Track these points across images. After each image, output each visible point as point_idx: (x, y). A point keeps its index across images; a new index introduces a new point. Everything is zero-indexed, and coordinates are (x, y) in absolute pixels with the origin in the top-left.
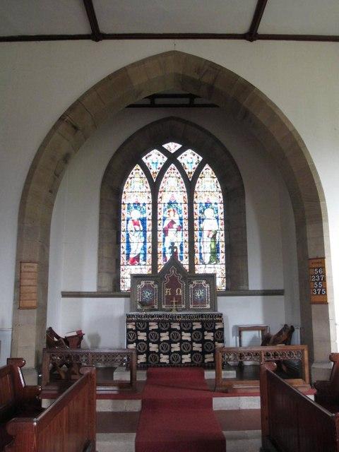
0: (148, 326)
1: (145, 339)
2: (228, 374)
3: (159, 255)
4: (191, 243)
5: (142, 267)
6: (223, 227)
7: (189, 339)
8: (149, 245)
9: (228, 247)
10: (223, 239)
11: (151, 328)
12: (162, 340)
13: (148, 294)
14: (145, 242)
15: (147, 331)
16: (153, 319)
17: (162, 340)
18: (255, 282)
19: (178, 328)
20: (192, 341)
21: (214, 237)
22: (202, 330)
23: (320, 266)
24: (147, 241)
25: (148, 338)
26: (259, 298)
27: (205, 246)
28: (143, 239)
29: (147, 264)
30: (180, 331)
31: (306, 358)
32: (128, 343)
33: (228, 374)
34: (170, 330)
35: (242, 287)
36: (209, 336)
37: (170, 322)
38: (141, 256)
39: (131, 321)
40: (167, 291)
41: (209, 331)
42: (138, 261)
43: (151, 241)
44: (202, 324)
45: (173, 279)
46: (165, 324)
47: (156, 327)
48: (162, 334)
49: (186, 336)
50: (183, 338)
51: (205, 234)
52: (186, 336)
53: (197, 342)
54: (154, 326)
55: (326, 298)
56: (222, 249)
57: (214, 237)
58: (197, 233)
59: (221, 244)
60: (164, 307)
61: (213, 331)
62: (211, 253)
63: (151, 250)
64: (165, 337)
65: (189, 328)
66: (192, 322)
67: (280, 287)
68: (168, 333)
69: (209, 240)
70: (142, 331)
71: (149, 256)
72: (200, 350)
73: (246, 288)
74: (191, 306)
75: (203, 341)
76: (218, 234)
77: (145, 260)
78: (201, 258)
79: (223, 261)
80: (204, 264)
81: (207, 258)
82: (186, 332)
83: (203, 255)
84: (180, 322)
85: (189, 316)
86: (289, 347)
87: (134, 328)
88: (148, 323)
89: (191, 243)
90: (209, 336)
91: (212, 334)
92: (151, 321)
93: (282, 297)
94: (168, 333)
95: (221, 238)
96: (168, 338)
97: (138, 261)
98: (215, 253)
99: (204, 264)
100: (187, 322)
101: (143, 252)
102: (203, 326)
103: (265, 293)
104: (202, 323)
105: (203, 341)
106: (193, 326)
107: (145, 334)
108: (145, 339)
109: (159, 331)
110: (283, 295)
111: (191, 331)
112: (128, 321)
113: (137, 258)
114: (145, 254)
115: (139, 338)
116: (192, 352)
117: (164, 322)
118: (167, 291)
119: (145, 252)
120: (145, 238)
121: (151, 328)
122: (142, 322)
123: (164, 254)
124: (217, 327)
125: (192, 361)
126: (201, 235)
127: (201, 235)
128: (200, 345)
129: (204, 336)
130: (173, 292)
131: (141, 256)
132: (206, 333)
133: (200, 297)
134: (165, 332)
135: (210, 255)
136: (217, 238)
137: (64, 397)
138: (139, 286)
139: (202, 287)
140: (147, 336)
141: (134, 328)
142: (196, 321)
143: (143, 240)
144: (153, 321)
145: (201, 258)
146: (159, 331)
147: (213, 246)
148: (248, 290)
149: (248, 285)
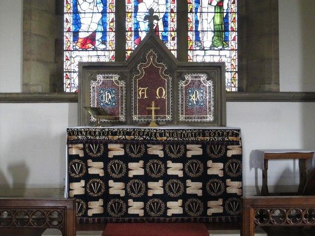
0: (107, 150)
9: (241, 20)
11: (111, 155)
12: (131, 174)
14: (104, 13)
15: (104, 158)
16: (116, 138)
17: (131, 174)
19: (161, 154)
26: (296, 106)
30: (164, 160)
34: (147, 158)
36: (216, 169)
37: (146, 143)
38: (99, 36)
39: (77, 142)
44: (204, 148)
45: (152, 71)
47: (121, 152)
49: (175, 169)
50: (170, 172)
52: (175, 169)
53: (194, 180)
54: (117, 150)
56: (233, 25)
61: (224, 159)
63: (113, 25)
69: (212, 9)
70: (95, 160)
71: (111, 36)
74: (182, 118)
75: (204, 178)
78: (198, 39)
79: (234, 44)
81: (208, 39)
82: (175, 161)
83: (200, 35)
85: (181, 133)
87: (81, 155)
88: (106, 144)
90: (216, 169)
92: (112, 142)
94: (141, 162)
98: (221, 32)
101: (101, 28)
102: (204, 151)
104: (204, 145)
105: (204, 178)
107: (101, 164)
109: (126, 159)
111: (183, 159)
113: (91, 39)
115: (91, 171)
116: (185, 197)
117: (133, 142)
121: (111, 155)
122: (96, 142)
124: (230, 154)
128: (200, 184)
131: (99, 36)
135: (211, 35)
138: (94, 84)
140: (105, 169)
141: (81, 155)
142: (192, 143)
143: (101, 9)
144: (116, 142)
146: (126, 159)
147: (218, 20)
148: (278, 92)
149: (278, 84)
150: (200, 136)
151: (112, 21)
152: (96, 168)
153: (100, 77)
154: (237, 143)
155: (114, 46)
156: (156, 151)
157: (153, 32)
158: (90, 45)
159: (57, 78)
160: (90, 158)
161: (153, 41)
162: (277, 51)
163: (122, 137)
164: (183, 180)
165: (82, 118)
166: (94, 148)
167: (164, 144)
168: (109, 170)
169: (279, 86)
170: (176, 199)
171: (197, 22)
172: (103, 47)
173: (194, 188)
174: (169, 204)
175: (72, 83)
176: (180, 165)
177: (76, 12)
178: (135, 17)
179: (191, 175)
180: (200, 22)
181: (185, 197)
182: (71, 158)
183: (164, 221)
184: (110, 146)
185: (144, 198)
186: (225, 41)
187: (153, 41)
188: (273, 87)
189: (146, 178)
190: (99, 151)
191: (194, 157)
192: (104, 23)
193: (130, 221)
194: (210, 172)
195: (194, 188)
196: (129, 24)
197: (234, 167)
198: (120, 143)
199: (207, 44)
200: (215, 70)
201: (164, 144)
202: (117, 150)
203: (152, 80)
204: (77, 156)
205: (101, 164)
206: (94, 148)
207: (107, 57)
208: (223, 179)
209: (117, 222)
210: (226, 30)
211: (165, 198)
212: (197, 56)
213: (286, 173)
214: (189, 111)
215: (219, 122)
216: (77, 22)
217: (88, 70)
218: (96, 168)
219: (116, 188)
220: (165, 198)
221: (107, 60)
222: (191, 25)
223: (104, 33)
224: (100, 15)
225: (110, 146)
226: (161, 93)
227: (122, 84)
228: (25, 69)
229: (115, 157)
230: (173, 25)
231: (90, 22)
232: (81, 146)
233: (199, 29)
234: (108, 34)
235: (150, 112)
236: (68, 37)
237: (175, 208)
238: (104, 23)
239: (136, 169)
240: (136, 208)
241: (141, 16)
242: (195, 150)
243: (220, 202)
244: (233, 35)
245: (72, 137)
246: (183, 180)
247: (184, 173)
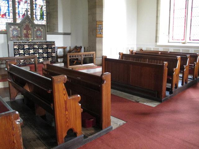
0: (24, 47)
1: (23, 53)
2: (61, 65)
3: (17, 14)
4: (32, 9)
5: (8, 19)
6: (45, 4)
7: (42, 52)
8: (11, 8)
9: (47, 13)
10: (45, 9)
11: (25, 48)
12: (30, 53)
13: (15, 33)
14: (8, 7)
15: (23, 49)
16: (27, 43)
17: (30, 53)
18: (60, 29)
19: (37, 47)
20: (43, 53)
21: (42, 8)
22: (47, 48)
23: (101, 24)
24: (10, 6)
25: (24, 52)
26: (62, 36)
27: (38, 13)
28: (7, 5)
29: (11, 18)
30: (38, 49)
31: (95, 56)
32: (15, 55)
33: (61, 65)
34: (34, 48)
35: (55, 31)
36: (50, 51)
37: (34, 45)
38: (7, 14)
39: (16, 45)
40: (25, 32)
41: (49, 49)
42: (6, 16)
43: (12, 6)
44: (47, 46)
45: (27, 26)
46: (31, 46)
47: (28, 47)
48: (30, 50)
49: (41, 51)
50: (40, 52)
51: (38, 6)
52: (41, 51)
53: (45, 53)
54: (26, 47)
55: (102, 36)
56: (45, 14)
57: (42, 8)
58: (34, 6)
59: (44, 12)
60: (23, 39)
61: (51, 48)
62: (40, 15)
63: (12, 11)
64: (32, 51)
65: (42, 47)
66: (43, 45)
67: (69, 32)
68: (33, 50)
69: (40, 9)
70: (21, 49)
71: (11, 15)
72: (46, 56)
73: (57, 32)
74: (35, 39)
75: (47, 53)
76: (43, 7)
77: (9, 16)
78: (36, 17)
79: (45, 19)
80: (38, 20)
81: (39, 17)
82: (40, 49)
83: (37, 16)
84: (38, 45)
85: (42, 42)
86: (80, 53)
87: (17, 48)
88: (24, 45)
89: (32, 9)
90: (50, 51)
91: (51, 50)
92: (25, 45)
93: (70, 36)
94: (33, 50)
95: (44, 9)
96: (33, 52)
97: (6, 16)
98: (42, 16)
99: (38, 20)
100: (41, 45)
101: (8, 12)
102: (47, 47)
103: (64, 34)
104: (47, 45)
105: (47, 53)
106: (43, 46)
107: (23, 51)
108: (23, 53)
109: (29, 49)
110: (70, 35)
111: (42, 49)
112: (14, 45)
113: (5, 15)
114: (9, 13)
115: (20, 52)
116: (43, 57)
117: (31, 45)
118: (25, 32)
119: (9, 11)
120: (9, 4)
121: (25, 48)
122: (21, 45)
123: (19, 14)
124: (53, 47)
125: (52, 60)
126: (36, 7)
127: (36, 7)
128: (46, 54)
129: (48, 50)
130: (27, 32)
131: (7, 14)
132: (48, 49)
133: (39, 35)
134: (31, 49)
135: (40, 16)
136: (43, 9)
137: (28, 79)
138: (11, 29)
139: (40, 30)
140: (24, 52)
141: (17, 48)
142: (44, 44)
143: (7, 6)
144: (26, 45)
145: (36, 17)
146: (29, 49)
147: (41, 13)
148: (58, 32)
149: (58, 30)
151: (11, 10)
152: (21, 52)
153: (12, 27)
154: (54, 44)
155: (12, 17)
158: (5, 17)
160: (39, 48)
162: (58, 23)
163: (28, 43)
164: (43, 53)
166: (21, 47)
167: (38, 45)
168: (25, 52)
170: (41, 58)
171: (36, 12)
172: (9, 17)
173: (45, 55)
174: (40, 59)
176: (42, 50)
178: (18, 9)
179: (44, 52)
180: (166, 67)
182: (14, 49)
183: (39, 63)
184: (25, 46)
188: (57, 31)
190: (22, 47)
191: (45, 48)
193: (31, 64)
194: (48, 51)
195: (45, 55)
196: (17, 11)
197: (54, 50)
198: (28, 45)
201: (38, 45)
202: (26, 47)
204: (16, 49)
205: (23, 51)
206: (21, 47)
208: (51, 53)
209: (28, 65)
210: (43, 15)
212: (36, 22)
213: (60, 51)
217: (37, 56)
221: (19, 22)
222: (34, 13)
223: (9, 13)
224: (7, 8)
225: (25, 46)
226: (30, 32)
227: (19, 29)
229: (26, 49)
232: (17, 46)
233: (36, 15)
234: (10, 13)
235: (29, 37)
238: (9, 10)
239: (32, 51)
243: (51, 58)
244: (45, 17)
246: (43, 53)
247: (43, 52)
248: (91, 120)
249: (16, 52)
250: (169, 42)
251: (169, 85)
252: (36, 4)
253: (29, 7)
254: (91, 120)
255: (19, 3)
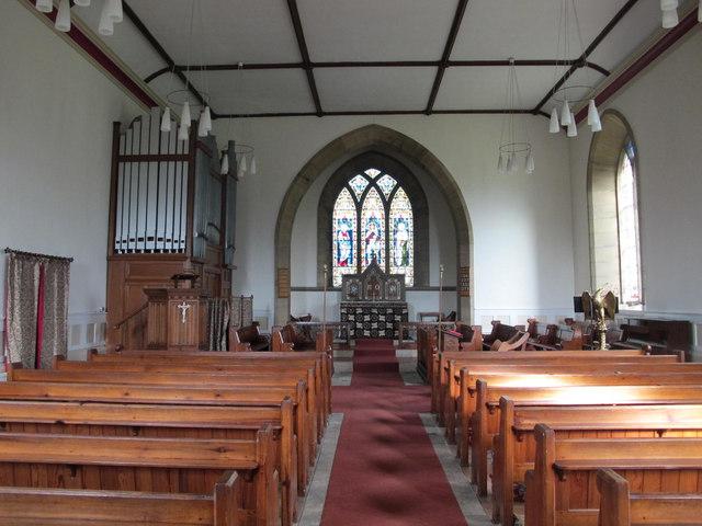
8: (355, 251)
15: (355, 314)
21: (405, 245)
22: (393, 314)
27: (398, 253)
36: (398, 318)
49: (382, 318)
51: (398, 243)
52: (382, 318)
54: (359, 311)
56: (411, 255)
57: (405, 245)
58: (391, 243)
61: (401, 314)
71: (355, 260)
81: (399, 262)
90: (398, 318)
95: (410, 246)
98: (405, 258)
105: (393, 322)
109: (363, 314)
111: (385, 314)
113: (346, 262)
118: (369, 287)
146: (363, 314)
150: (391, 305)
152: (351, 318)
156: (375, 311)
157: (374, 260)
159: (330, 279)
161: (374, 264)
165: (344, 298)
169: (306, 190)
173: (389, 325)
175: (338, 282)
177: (339, 249)
181: (386, 329)
185: (370, 329)
186: (407, 263)
187: (374, 264)
189: (370, 322)
192: (351, 254)
195: (389, 325)
196: (363, 255)
199: (399, 263)
200: (401, 277)
202: (359, 311)
203: (373, 282)
207: (353, 271)
211: (378, 329)
212: (394, 271)
214: (390, 295)
215: (132, 277)
216: (339, 254)
217: (346, 277)
218: (351, 318)
219: (359, 325)
220: (378, 329)
228: (318, 277)
230: (383, 255)
231: (345, 254)
236: (335, 261)
237: (382, 333)
238: (351, 254)
239: (367, 318)
240: (367, 333)
241: (369, 252)
242: (390, 311)
244: (411, 260)
245: (611, 299)
248: (489, 456)
249: (344, 319)
250: (455, 293)
251: (447, 366)
252: (395, 240)
253: (384, 246)
254: (489, 456)
255: (367, 241)
